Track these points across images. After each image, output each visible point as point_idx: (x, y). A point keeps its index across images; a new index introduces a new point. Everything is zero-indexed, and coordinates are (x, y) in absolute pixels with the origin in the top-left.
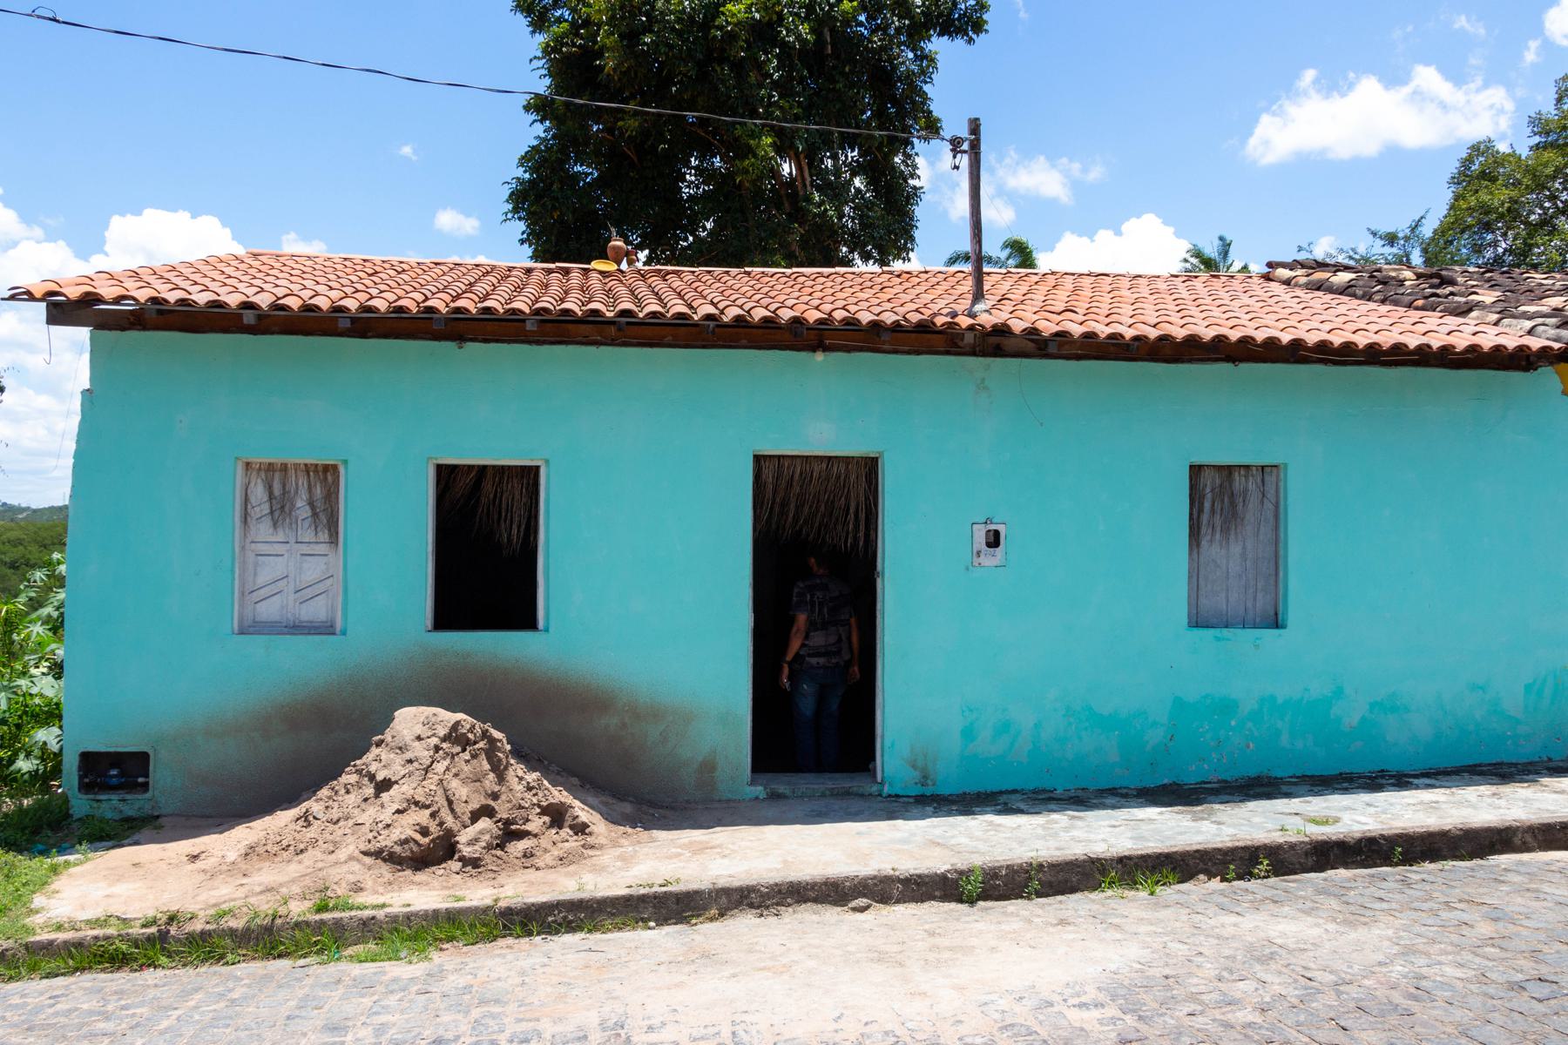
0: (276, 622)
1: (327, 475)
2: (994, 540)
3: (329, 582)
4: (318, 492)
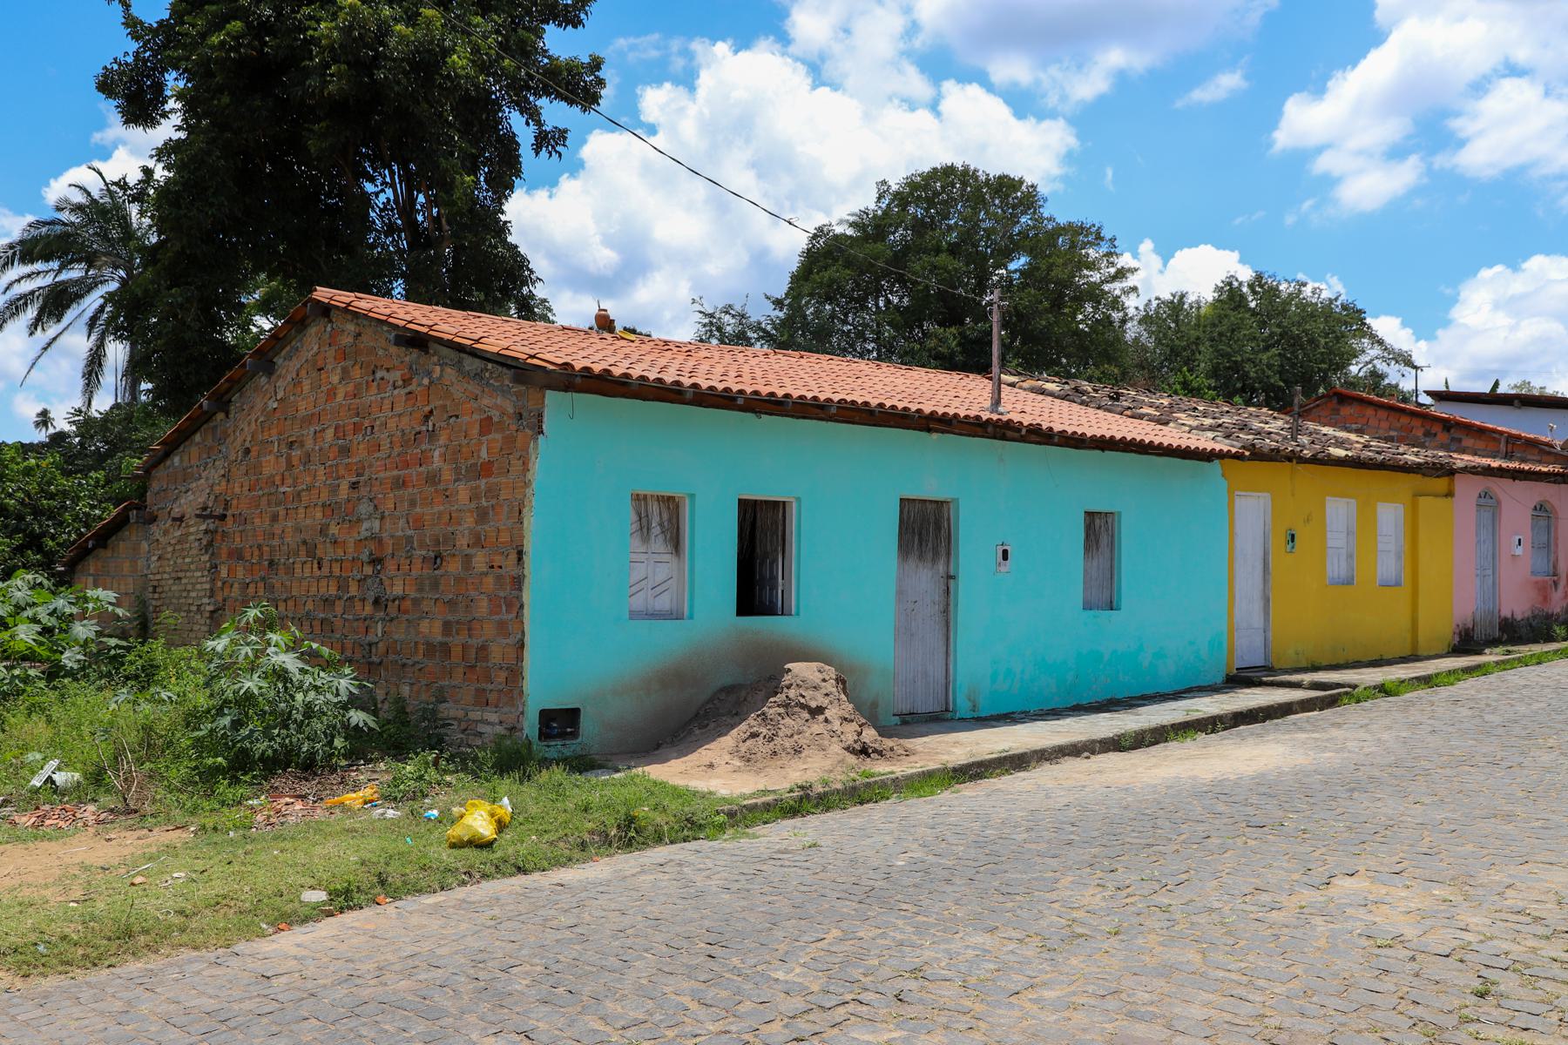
1: (671, 504)
2: (1005, 555)
3: (669, 582)
4: (665, 516)
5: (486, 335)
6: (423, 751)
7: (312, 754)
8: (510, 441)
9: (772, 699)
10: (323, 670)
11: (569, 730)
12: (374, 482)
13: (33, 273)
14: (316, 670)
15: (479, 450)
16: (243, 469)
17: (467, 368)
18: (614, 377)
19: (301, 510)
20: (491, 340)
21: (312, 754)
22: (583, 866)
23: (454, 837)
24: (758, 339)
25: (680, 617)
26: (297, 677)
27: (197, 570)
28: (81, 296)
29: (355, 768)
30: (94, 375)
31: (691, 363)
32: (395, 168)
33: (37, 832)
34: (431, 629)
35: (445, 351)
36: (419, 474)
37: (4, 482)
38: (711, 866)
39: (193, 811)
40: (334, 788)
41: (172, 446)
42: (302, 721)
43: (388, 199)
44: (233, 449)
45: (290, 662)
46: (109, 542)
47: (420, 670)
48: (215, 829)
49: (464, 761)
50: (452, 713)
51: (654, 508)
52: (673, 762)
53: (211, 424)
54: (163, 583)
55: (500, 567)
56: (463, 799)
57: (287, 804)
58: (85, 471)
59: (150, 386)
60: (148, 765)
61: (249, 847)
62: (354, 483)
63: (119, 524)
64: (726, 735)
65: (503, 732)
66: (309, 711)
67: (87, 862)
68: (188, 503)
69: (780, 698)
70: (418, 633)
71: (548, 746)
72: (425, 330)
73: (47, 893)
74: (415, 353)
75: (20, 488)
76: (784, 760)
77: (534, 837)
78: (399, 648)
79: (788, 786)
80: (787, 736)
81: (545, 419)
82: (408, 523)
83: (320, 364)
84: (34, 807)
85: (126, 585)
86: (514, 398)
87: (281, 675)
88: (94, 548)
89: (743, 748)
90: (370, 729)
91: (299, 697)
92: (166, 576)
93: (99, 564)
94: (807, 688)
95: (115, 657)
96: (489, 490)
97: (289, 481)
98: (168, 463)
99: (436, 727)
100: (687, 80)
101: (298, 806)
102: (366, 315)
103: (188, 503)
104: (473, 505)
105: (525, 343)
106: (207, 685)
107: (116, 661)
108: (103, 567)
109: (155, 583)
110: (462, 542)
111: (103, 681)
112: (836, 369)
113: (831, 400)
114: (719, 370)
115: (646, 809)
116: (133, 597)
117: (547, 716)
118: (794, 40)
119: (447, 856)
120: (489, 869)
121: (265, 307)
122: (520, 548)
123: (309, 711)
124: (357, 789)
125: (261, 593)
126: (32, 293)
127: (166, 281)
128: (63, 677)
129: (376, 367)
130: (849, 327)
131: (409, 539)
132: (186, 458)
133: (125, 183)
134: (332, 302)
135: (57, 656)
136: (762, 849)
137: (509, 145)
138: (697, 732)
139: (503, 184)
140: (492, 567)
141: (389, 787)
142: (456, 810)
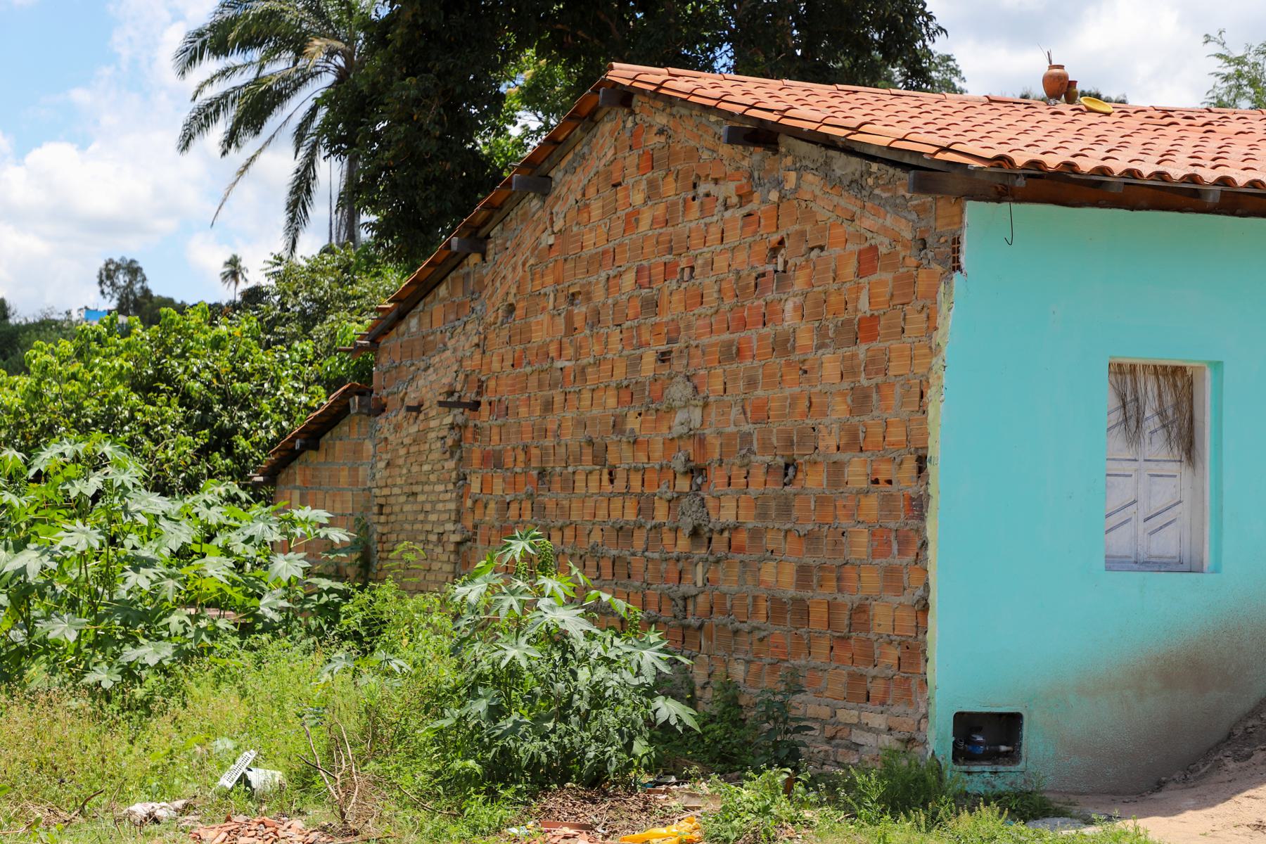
0: (1126, 557)
3: (1178, 508)
4: (1169, 400)
5: (868, 119)
6: (770, 767)
8: (906, 283)
10: (618, 635)
11: (1003, 748)
12: (693, 351)
14: (609, 635)
15: (858, 298)
16: (505, 333)
17: (839, 172)
19: (586, 395)
20: (878, 127)
21: (602, 763)
26: (580, 644)
27: (439, 481)
29: (663, 788)
30: (300, 206)
31: (1213, 144)
35: (803, 148)
36: (761, 338)
40: (634, 817)
42: (588, 712)
44: (491, 306)
45: (572, 621)
46: (322, 441)
47: (761, 640)
51: (1149, 387)
52: (1189, 815)
53: (462, 271)
54: (392, 500)
55: (890, 482)
59: (374, 218)
60: (372, 765)
62: (663, 354)
65: (897, 746)
66: (598, 697)
71: (969, 773)
74: (757, 154)
75: (207, 367)
78: (728, 605)
81: (964, 247)
82: (745, 413)
83: (616, 177)
85: (343, 502)
86: (914, 216)
87: (557, 639)
88: (304, 448)
91: (584, 674)
92: (396, 491)
96: (871, 361)
97: (569, 351)
98: (403, 328)
99: (787, 732)
102: (685, 100)
104: (846, 385)
105: (931, 128)
106: (455, 651)
107: (330, 612)
109: (382, 501)
110: (829, 442)
111: (311, 640)
117: (966, 724)
121: (533, 96)
122: (920, 452)
124: (667, 821)
125: (527, 516)
126: (225, 95)
127: (400, 69)
128: (261, 632)
129: (698, 177)
131: (746, 438)
134: (636, 84)
135: (254, 601)
138: (1232, 765)
140: (876, 482)
141: (717, 821)
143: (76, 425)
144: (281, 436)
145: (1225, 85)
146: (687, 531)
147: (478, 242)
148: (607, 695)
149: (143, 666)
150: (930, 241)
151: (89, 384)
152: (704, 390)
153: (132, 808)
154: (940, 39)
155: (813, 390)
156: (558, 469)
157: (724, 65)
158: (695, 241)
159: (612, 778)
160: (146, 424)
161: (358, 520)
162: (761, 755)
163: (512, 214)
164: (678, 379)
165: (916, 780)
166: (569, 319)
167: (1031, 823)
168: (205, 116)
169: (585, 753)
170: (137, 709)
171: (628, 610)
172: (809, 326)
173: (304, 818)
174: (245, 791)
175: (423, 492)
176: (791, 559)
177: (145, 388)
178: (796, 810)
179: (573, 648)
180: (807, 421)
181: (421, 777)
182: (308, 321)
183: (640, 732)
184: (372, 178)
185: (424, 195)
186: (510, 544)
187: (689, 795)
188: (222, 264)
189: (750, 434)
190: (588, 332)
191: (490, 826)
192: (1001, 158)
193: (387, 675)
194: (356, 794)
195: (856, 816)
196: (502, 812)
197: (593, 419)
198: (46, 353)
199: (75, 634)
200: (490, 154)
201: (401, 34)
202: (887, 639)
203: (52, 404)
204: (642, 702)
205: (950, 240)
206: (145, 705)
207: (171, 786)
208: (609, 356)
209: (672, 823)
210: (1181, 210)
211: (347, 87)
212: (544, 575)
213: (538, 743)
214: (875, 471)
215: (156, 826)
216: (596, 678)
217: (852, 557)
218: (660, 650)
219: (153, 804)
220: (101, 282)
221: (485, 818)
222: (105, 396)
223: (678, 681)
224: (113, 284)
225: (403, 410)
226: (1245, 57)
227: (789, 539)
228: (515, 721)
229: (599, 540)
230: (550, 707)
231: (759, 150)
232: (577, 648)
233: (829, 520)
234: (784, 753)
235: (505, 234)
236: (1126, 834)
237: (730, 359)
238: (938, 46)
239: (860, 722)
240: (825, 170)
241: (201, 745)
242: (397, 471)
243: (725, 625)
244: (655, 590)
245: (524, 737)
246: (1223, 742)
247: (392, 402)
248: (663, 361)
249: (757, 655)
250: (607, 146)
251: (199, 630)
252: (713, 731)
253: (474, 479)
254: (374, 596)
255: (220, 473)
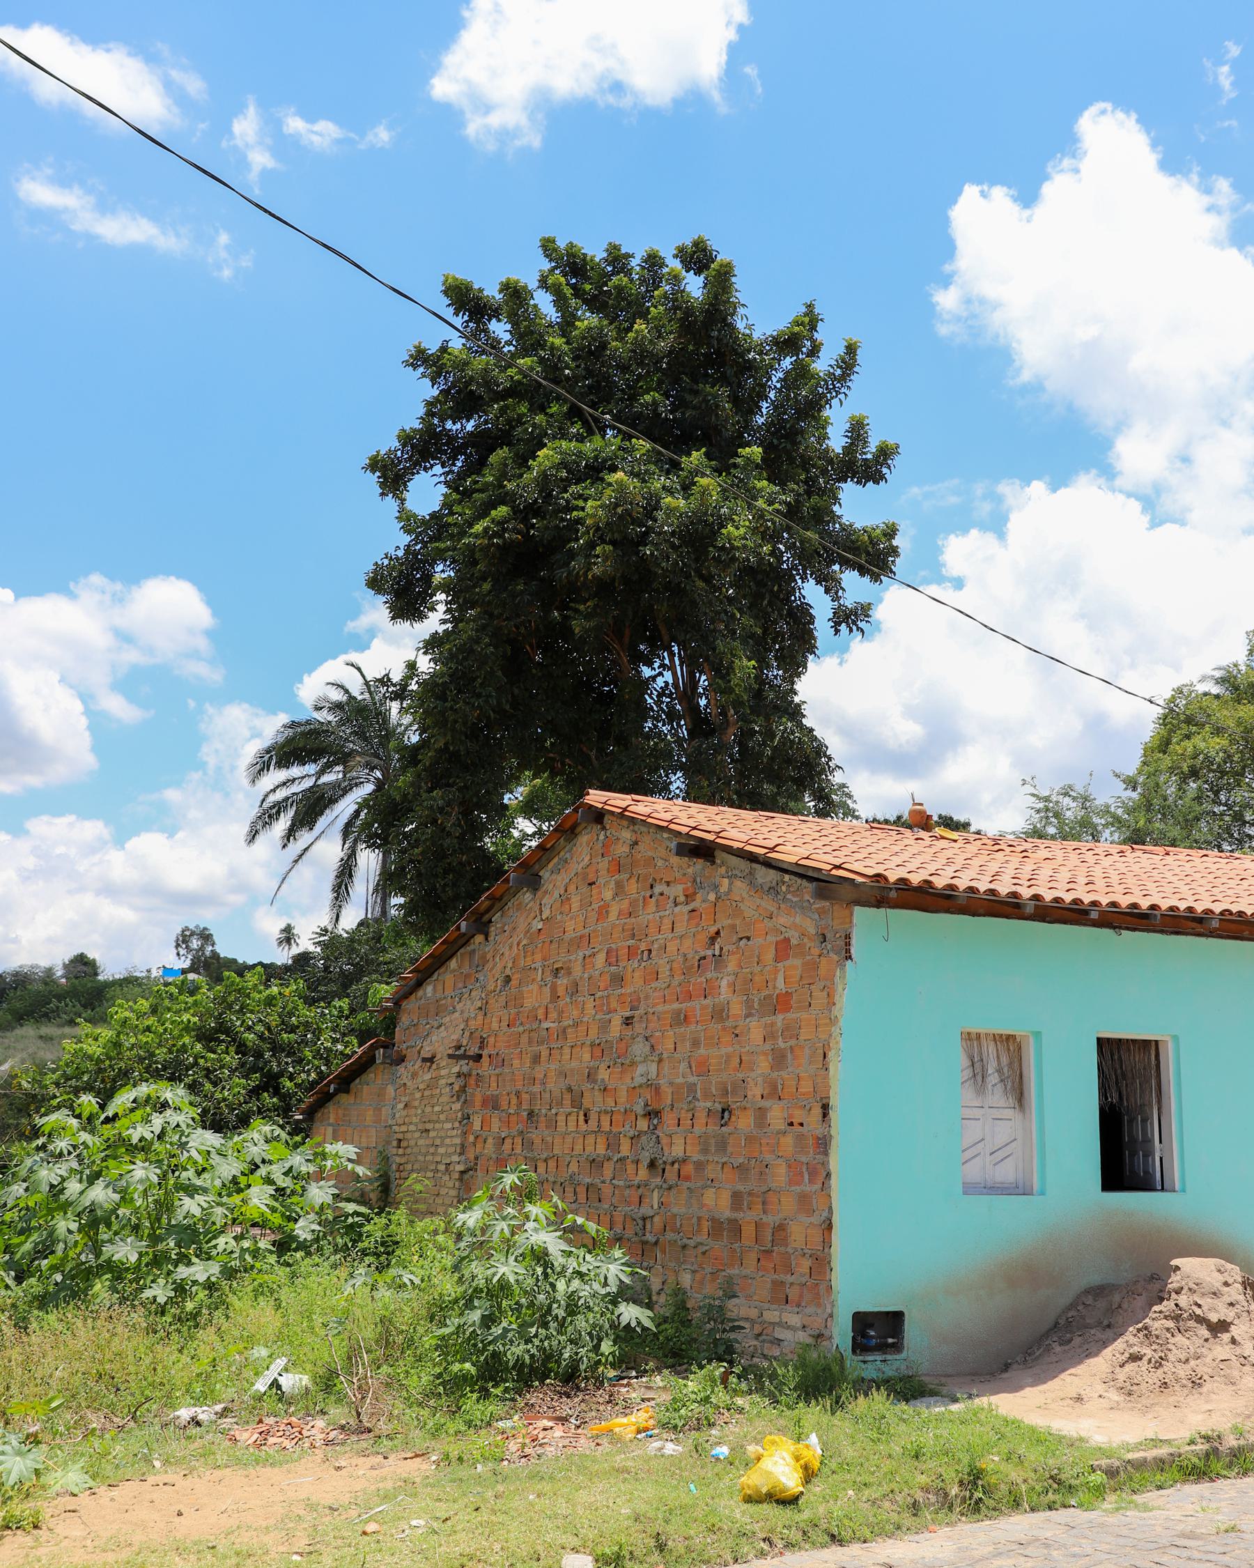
1: (1011, 1045)
3: (1014, 1144)
4: (1005, 1060)
5: (780, 841)
6: (710, 1362)
7: (575, 1363)
8: (813, 967)
9: (1156, 1308)
10: (590, 1252)
11: (890, 1340)
12: (650, 1016)
13: (289, 781)
14: (582, 1252)
15: (776, 978)
16: (502, 1000)
17: (760, 881)
18: (936, 889)
19: (567, 1051)
20: (788, 848)
21: (575, 1363)
22: (917, 1537)
23: (749, 1487)
24: (1106, 826)
25: (1027, 1192)
26: (558, 1260)
27: (447, 1120)
28: (336, 801)
29: (625, 1382)
30: (343, 887)
31: (1028, 867)
32: (676, 649)
33: (259, 1456)
34: (718, 1202)
35: (734, 861)
36: (703, 1008)
37: (244, 1014)
38: (1089, 1551)
39: (435, 1433)
40: (601, 1408)
41: (425, 973)
42: (564, 1318)
43: (666, 683)
44: (491, 977)
45: (552, 1242)
46: (352, 1085)
47: (704, 1253)
48: (460, 1459)
49: (759, 1378)
50: (743, 1313)
51: (990, 1050)
52: (1028, 1391)
53: (469, 948)
54: (408, 1136)
55: (801, 1125)
56: (759, 1433)
57: (545, 1429)
58: (328, 999)
59: (401, 900)
60: (385, 1369)
61: (500, 1488)
62: (627, 1018)
63: (363, 1066)
64: (1096, 1355)
65: (810, 1341)
66: (573, 1308)
67: (314, 1499)
68: (440, 1041)
69: (1167, 1306)
70: (703, 1206)
71: (865, 1362)
72: (711, 837)
73: (268, 1540)
74: (700, 863)
75: (260, 1021)
76: (1178, 1395)
77: (851, 1492)
78: (678, 1224)
79: (1186, 1434)
80: (1180, 1361)
81: (853, 942)
82: (691, 1068)
83: (591, 878)
84: (257, 1419)
85: (368, 1137)
86: (817, 916)
87: (540, 1256)
88: (337, 1092)
89: (1122, 1374)
90: (645, 1329)
91: (561, 1285)
92: (412, 1128)
93: (340, 1112)
94: (1203, 1294)
95: (352, 1225)
96: (786, 1028)
97: (553, 1015)
98: (420, 993)
99: (724, 1331)
100: (997, 525)
101: (558, 1432)
102: (644, 821)
103: (440, 1041)
104: (768, 1046)
105: (828, 849)
106: (456, 1268)
107: (354, 1232)
108: (344, 1116)
109: (400, 1136)
110: (755, 1091)
111: (338, 1256)
112: (1213, 868)
113: (1212, 912)
114: (1064, 875)
115: (996, 1459)
116: (375, 1153)
117: (862, 1321)
118: (1121, 473)
119: (742, 1514)
120: (795, 1536)
121: (530, 808)
122: (824, 1101)
123: (573, 1308)
124: (628, 1411)
125: (518, 1150)
126: (287, 798)
127: (426, 783)
128: (296, 1250)
129: (655, 880)
130: (1222, 808)
131: (692, 1088)
132: (440, 987)
133: (389, 680)
134: (606, 807)
135: (291, 1225)
136: (1159, 1529)
137: (801, 619)
138: (1058, 1349)
139: (794, 665)
140: (791, 1124)
141: (668, 1410)
142: (752, 1449)
143: (147, 1070)
144: (320, 1078)
145: (1038, 816)
146: (646, 1163)
147: (482, 925)
148: (580, 1304)
149: (195, 1282)
150: (828, 936)
151: (161, 1036)
152: (659, 1049)
153: (176, 1413)
154: (838, 773)
155: (743, 1050)
156: (544, 1111)
157: (678, 788)
158: (652, 930)
159: (583, 1374)
160: (207, 1069)
161: (381, 1152)
162: (704, 1351)
163: (510, 904)
164: (638, 1039)
165: (824, 1369)
166: (554, 989)
167: (912, 1402)
168: (269, 815)
169: (562, 1355)
170: (188, 1320)
171: (598, 1231)
172: (740, 999)
173: (326, 1417)
174: (276, 1394)
175: (434, 1129)
176: (727, 1186)
177: (207, 1037)
178: (731, 1398)
179: (553, 1265)
180: (739, 1075)
181: (425, 1379)
182: (347, 981)
183: (607, 1335)
184: (401, 870)
185: (442, 883)
186: (502, 1177)
187: (646, 1387)
188: (278, 932)
189: (695, 1085)
190: (568, 1000)
191: (482, 1421)
192: (878, 875)
193: (400, 1287)
194: (370, 1395)
195: (777, 1402)
196: (493, 1408)
197: (572, 1070)
198: (126, 1009)
199: (136, 1256)
200: (496, 851)
201: (430, 757)
202: (801, 1252)
203: (128, 1053)
204: (608, 1309)
205: (843, 936)
206: (195, 1315)
207: (212, 1391)
208: (585, 1019)
209: (632, 1412)
210: (1007, 917)
211: (382, 796)
212: (530, 1202)
213: (522, 1347)
214: (791, 1116)
215: (198, 1428)
216: (571, 1289)
217: (773, 1185)
218: (623, 1264)
219: (197, 1409)
220: (178, 946)
221: (478, 1413)
222: (174, 1045)
223: (638, 1288)
224: (187, 947)
225: (420, 1060)
226: (1050, 796)
227: (725, 1170)
228: (504, 1328)
229: (576, 1170)
230: (534, 1314)
231: (701, 861)
232: (556, 1264)
233: (756, 1155)
234: (721, 1349)
235: (504, 920)
236: (982, 1409)
237: (679, 1024)
238: (837, 778)
239: (781, 1321)
240: (750, 878)
241: (240, 1353)
242: (413, 1111)
243: (675, 1241)
244: (620, 1212)
245: (512, 1342)
246: (1051, 1330)
247: (412, 1054)
248: (627, 1024)
249: (700, 1266)
250: (584, 853)
251: (243, 1250)
252: (666, 1330)
253: (476, 1118)
254: (389, 1220)
255: (268, 1110)
